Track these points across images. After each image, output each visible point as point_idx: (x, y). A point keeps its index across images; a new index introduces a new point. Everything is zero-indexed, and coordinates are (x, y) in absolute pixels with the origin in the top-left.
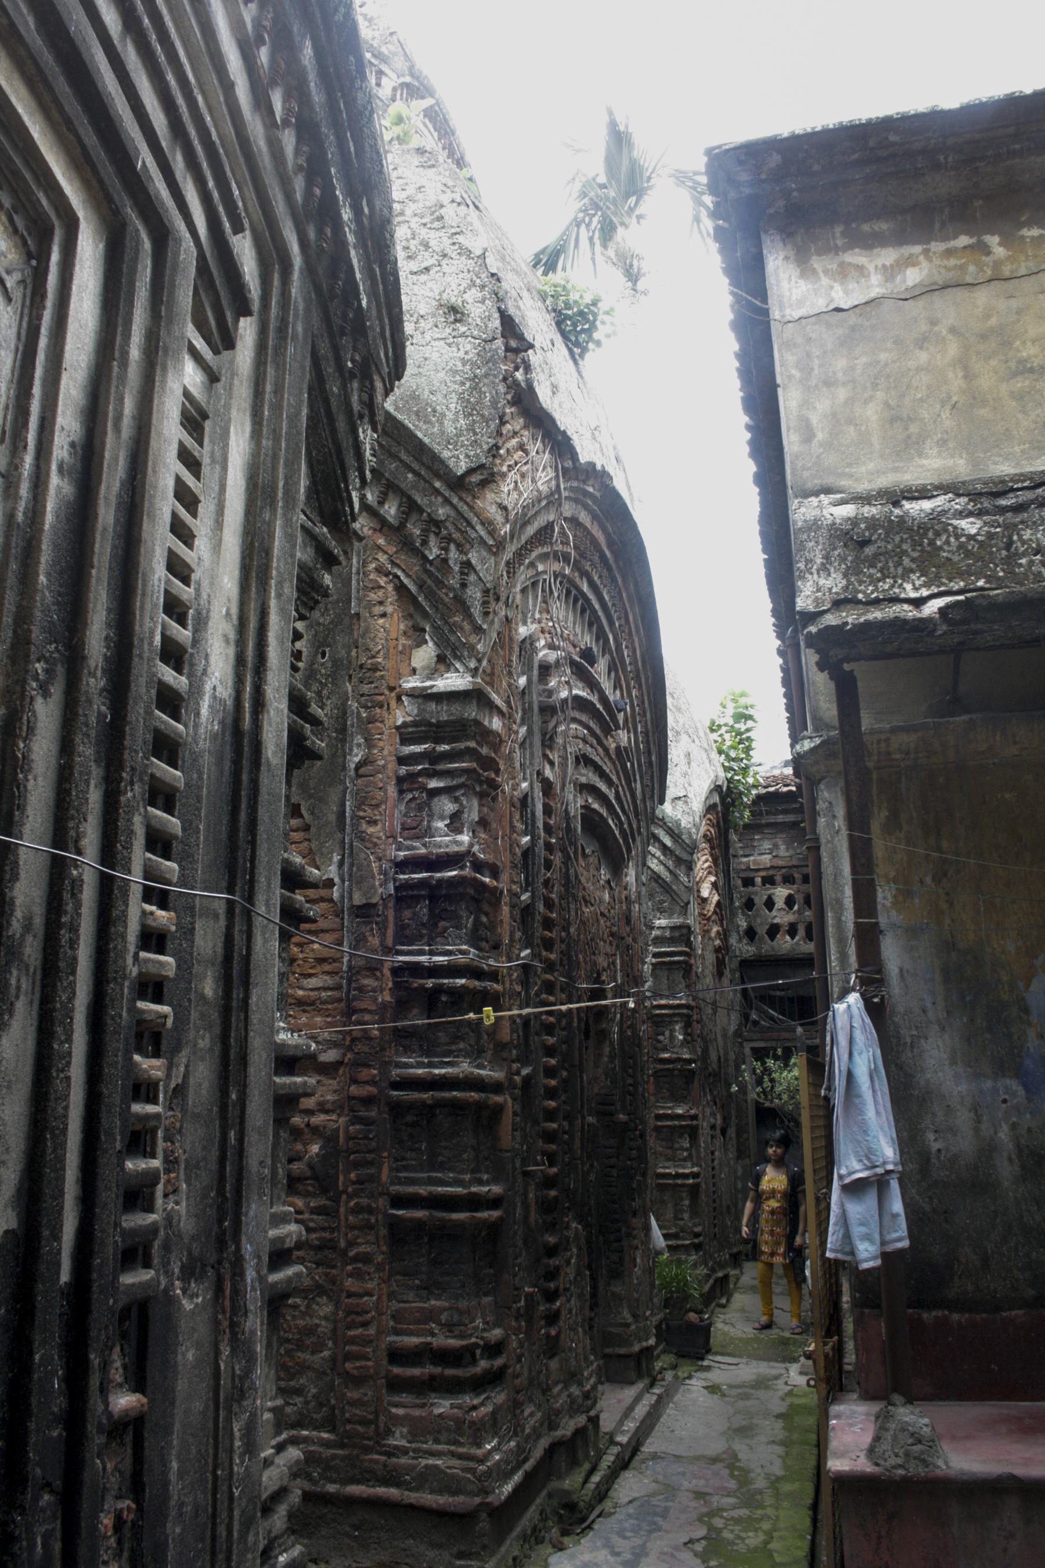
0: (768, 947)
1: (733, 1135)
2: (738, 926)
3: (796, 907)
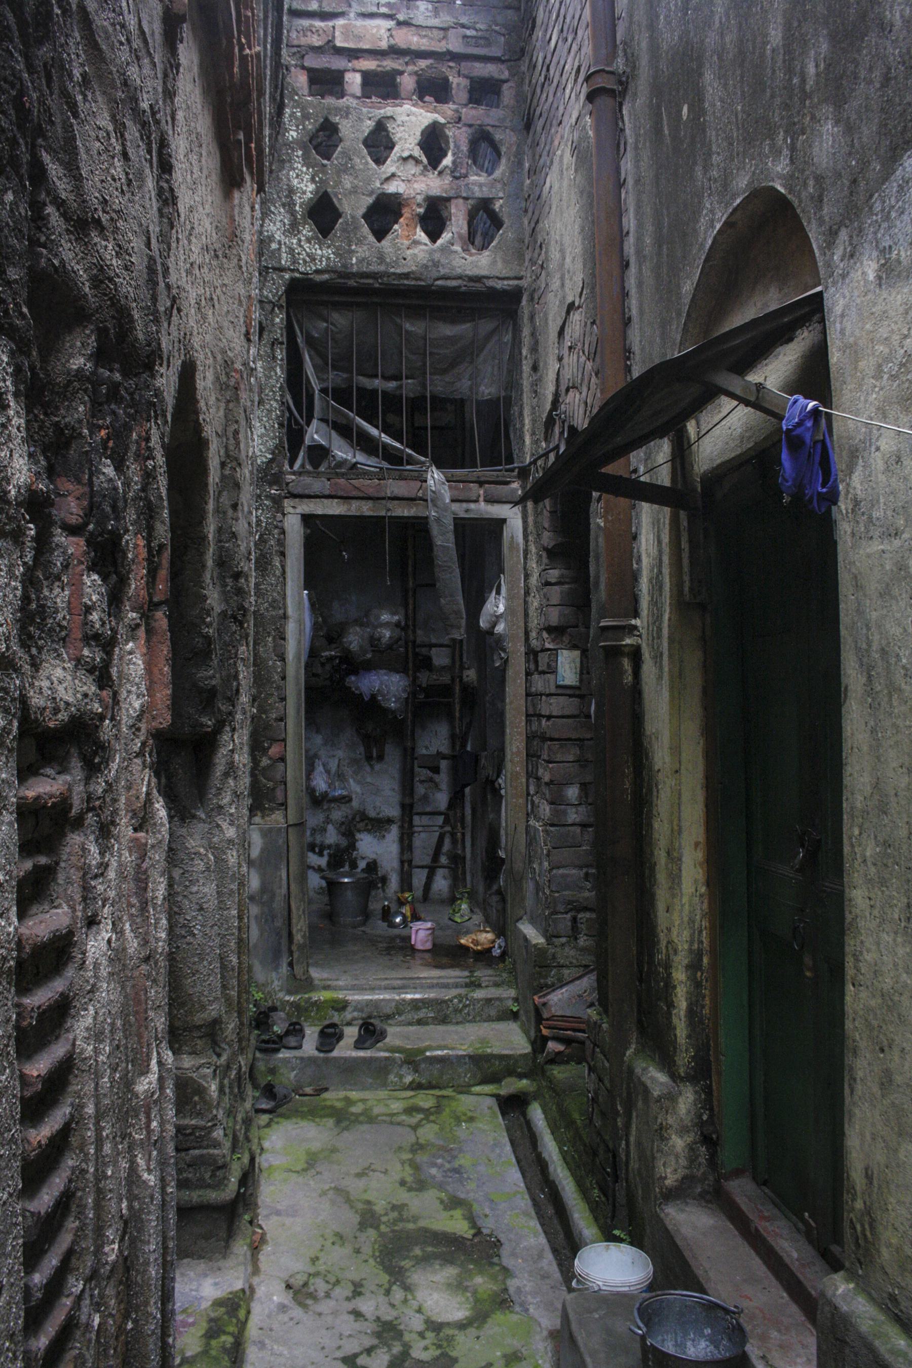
0: (364, 252)
1: (242, 759)
2: (291, 191)
3: (448, 161)
